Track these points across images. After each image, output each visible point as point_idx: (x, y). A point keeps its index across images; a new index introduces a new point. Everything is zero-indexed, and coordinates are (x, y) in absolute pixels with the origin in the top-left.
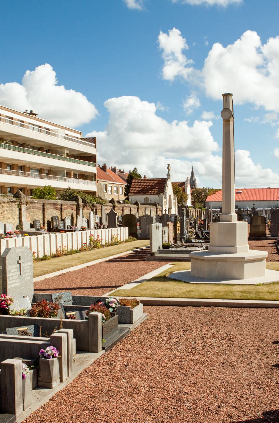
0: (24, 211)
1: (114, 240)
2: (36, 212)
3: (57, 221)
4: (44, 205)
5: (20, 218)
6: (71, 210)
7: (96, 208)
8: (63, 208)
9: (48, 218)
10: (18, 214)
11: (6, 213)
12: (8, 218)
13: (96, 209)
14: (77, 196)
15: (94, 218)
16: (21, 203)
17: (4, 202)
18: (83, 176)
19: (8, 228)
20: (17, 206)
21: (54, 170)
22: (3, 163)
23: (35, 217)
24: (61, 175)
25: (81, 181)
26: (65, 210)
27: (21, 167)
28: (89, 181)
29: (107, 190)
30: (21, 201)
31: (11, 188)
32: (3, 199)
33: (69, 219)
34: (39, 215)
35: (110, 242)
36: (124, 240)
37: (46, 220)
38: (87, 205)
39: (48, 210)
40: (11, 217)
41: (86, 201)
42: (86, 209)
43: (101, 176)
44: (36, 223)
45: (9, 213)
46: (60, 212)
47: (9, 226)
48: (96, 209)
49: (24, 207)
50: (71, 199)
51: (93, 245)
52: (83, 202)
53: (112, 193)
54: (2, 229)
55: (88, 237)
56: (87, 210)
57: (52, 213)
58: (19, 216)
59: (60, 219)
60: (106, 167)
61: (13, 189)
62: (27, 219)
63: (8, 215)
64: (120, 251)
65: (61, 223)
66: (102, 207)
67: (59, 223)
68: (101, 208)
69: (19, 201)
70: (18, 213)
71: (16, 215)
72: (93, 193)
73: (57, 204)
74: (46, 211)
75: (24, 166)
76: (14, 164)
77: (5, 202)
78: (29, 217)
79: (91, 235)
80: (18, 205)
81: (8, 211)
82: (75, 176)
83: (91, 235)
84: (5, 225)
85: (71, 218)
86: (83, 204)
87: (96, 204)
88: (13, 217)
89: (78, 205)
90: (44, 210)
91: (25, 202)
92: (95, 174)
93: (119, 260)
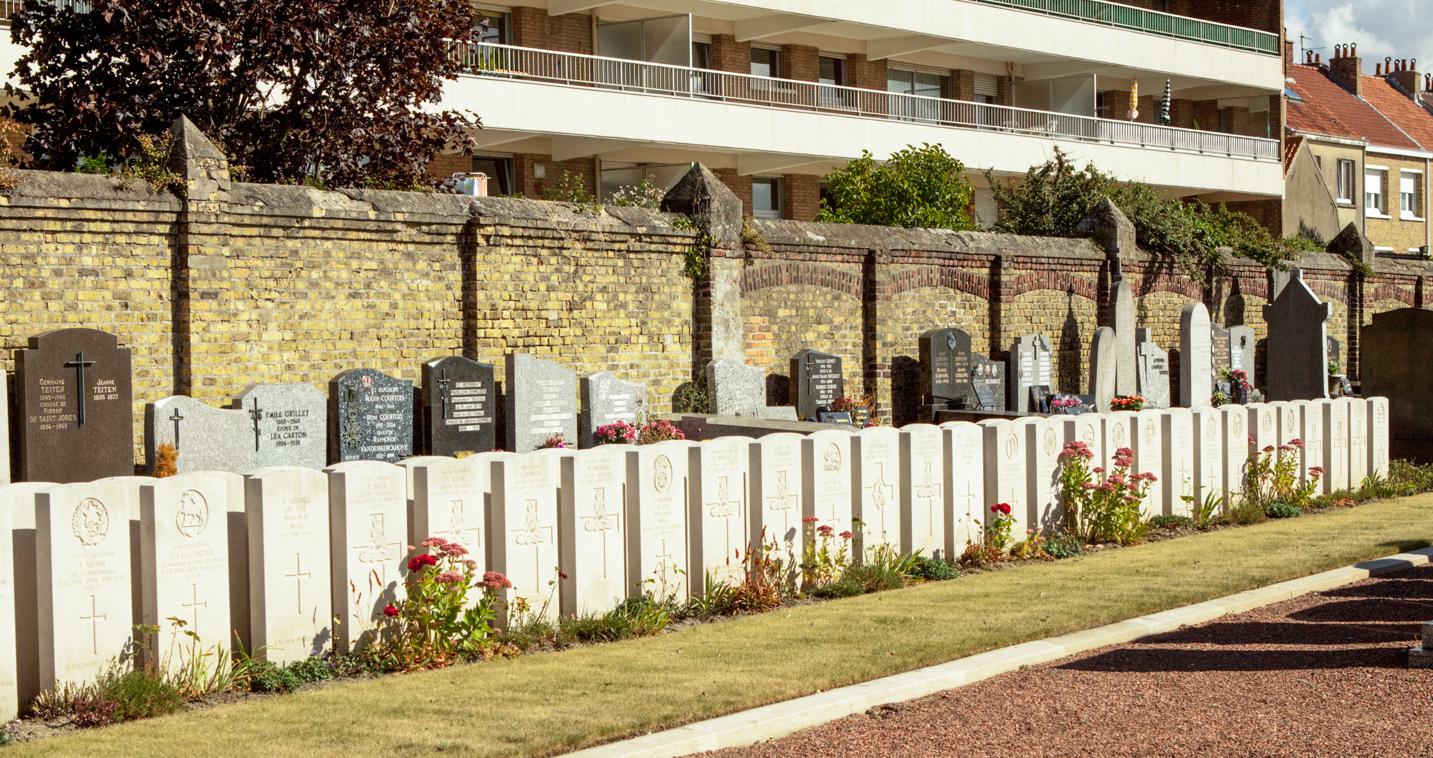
0: (729, 296)
1: (1266, 487)
2: (819, 304)
3: (960, 358)
4: (870, 261)
5: (703, 343)
6: (1063, 293)
7: (1235, 284)
8: (1004, 278)
9: (899, 337)
10: (688, 315)
11: (600, 305)
12: (617, 342)
13: (1236, 291)
14: (1107, 208)
15: (1213, 341)
16: (708, 245)
17: (585, 238)
18: (1205, 110)
19: (609, 404)
20: (683, 265)
21: (1027, 79)
22: (731, 38)
23: (811, 336)
24: (1069, 103)
25: (1184, 135)
26: (1019, 292)
27: (837, 63)
28: (1237, 141)
29: (1359, 194)
30: (704, 230)
31: (774, 183)
32: (580, 222)
33: (1044, 347)
34: (838, 320)
35: (1235, 501)
36: (1357, 486)
37: (884, 356)
38: (1171, 267)
39: (900, 289)
40: (637, 330)
41: (1162, 236)
42: (1168, 289)
43: (1325, 116)
44: (809, 374)
45: (624, 306)
46: (983, 305)
47: (614, 390)
48: (1236, 291)
49: (725, 274)
50: (1066, 228)
51: (1083, 525)
52: (1141, 243)
53: (1385, 212)
54: (563, 410)
55: (1047, 464)
56: (1175, 297)
57: (929, 313)
58: (697, 329)
59: (980, 345)
60: (1354, 60)
61: (788, 189)
62: (749, 346)
63: (617, 322)
64: (1257, 574)
65: (990, 376)
66: (1269, 274)
67: (973, 374)
68: (1265, 281)
69: (694, 232)
70: (685, 306)
71: (677, 321)
72: (1267, 210)
73: (965, 258)
74: (888, 299)
75: (852, 57)
76: (796, 47)
77: (594, 236)
78: (769, 335)
79: (1074, 447)
80: (690, 260)
81: (615, 297)
82: (1152, 111)
83: (1073, 451)
84: (585, 383)
85: (1063, 343)
86: (1146, 256)
87: (1235, 261)
88: (650, 337)
89: (1110, 267)
90: (873, 291)
91: (738, 240)
92: (1274, 98)
93: (1208, 647)
